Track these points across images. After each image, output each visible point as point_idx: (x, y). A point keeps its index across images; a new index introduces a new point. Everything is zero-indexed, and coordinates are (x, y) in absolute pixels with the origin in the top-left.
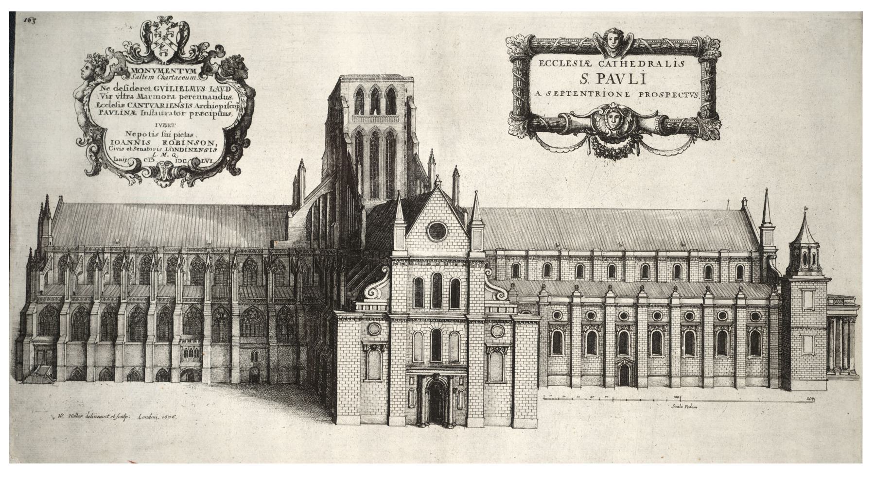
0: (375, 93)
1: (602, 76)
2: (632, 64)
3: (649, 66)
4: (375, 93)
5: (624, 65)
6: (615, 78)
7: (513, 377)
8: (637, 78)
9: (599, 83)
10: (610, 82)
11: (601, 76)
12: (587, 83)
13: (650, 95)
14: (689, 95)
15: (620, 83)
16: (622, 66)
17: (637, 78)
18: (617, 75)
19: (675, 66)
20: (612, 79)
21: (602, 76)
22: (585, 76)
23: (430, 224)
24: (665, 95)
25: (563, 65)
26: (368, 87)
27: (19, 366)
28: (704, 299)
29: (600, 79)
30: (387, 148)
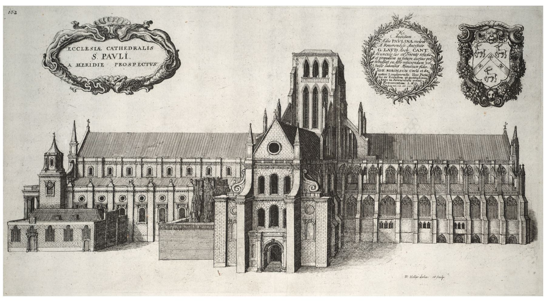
0: (316, 64)
1: (104, 55)
2: (125, 48)
3: (134, 49)
4: (316, 64)
5: (121, 49)
6: (112, 56)
7: (174, 210)
8: (123, 55)
9: (103, 59)
10: (109, 58)
11: (104, 55)
12: (96, 58)
13: (122, 64)
14: (149, 65)
15: (115, 58)
16: (120, 50)
17: (123, 55)
18: (113, 54)
19: (148, 49)
20: (110, 57)
21: (104, 55)
22: (95, 55)
23: (281, 147)
24: (132, 65)
25: (144, 49)
26: (311, 60)
27: (162, 218)
28: (142, 162)
29: (103, 56)
30: (313, 101)
